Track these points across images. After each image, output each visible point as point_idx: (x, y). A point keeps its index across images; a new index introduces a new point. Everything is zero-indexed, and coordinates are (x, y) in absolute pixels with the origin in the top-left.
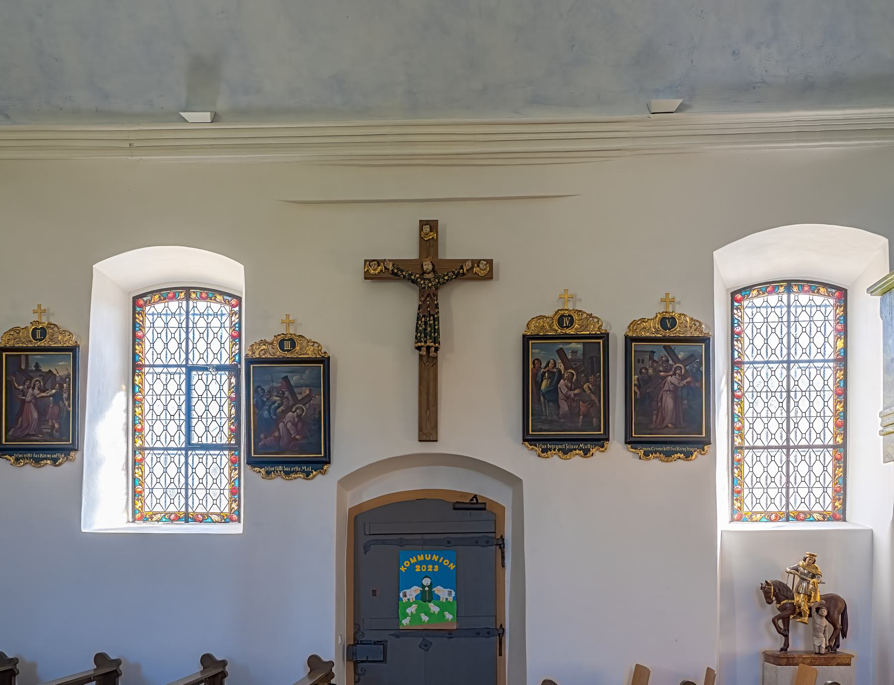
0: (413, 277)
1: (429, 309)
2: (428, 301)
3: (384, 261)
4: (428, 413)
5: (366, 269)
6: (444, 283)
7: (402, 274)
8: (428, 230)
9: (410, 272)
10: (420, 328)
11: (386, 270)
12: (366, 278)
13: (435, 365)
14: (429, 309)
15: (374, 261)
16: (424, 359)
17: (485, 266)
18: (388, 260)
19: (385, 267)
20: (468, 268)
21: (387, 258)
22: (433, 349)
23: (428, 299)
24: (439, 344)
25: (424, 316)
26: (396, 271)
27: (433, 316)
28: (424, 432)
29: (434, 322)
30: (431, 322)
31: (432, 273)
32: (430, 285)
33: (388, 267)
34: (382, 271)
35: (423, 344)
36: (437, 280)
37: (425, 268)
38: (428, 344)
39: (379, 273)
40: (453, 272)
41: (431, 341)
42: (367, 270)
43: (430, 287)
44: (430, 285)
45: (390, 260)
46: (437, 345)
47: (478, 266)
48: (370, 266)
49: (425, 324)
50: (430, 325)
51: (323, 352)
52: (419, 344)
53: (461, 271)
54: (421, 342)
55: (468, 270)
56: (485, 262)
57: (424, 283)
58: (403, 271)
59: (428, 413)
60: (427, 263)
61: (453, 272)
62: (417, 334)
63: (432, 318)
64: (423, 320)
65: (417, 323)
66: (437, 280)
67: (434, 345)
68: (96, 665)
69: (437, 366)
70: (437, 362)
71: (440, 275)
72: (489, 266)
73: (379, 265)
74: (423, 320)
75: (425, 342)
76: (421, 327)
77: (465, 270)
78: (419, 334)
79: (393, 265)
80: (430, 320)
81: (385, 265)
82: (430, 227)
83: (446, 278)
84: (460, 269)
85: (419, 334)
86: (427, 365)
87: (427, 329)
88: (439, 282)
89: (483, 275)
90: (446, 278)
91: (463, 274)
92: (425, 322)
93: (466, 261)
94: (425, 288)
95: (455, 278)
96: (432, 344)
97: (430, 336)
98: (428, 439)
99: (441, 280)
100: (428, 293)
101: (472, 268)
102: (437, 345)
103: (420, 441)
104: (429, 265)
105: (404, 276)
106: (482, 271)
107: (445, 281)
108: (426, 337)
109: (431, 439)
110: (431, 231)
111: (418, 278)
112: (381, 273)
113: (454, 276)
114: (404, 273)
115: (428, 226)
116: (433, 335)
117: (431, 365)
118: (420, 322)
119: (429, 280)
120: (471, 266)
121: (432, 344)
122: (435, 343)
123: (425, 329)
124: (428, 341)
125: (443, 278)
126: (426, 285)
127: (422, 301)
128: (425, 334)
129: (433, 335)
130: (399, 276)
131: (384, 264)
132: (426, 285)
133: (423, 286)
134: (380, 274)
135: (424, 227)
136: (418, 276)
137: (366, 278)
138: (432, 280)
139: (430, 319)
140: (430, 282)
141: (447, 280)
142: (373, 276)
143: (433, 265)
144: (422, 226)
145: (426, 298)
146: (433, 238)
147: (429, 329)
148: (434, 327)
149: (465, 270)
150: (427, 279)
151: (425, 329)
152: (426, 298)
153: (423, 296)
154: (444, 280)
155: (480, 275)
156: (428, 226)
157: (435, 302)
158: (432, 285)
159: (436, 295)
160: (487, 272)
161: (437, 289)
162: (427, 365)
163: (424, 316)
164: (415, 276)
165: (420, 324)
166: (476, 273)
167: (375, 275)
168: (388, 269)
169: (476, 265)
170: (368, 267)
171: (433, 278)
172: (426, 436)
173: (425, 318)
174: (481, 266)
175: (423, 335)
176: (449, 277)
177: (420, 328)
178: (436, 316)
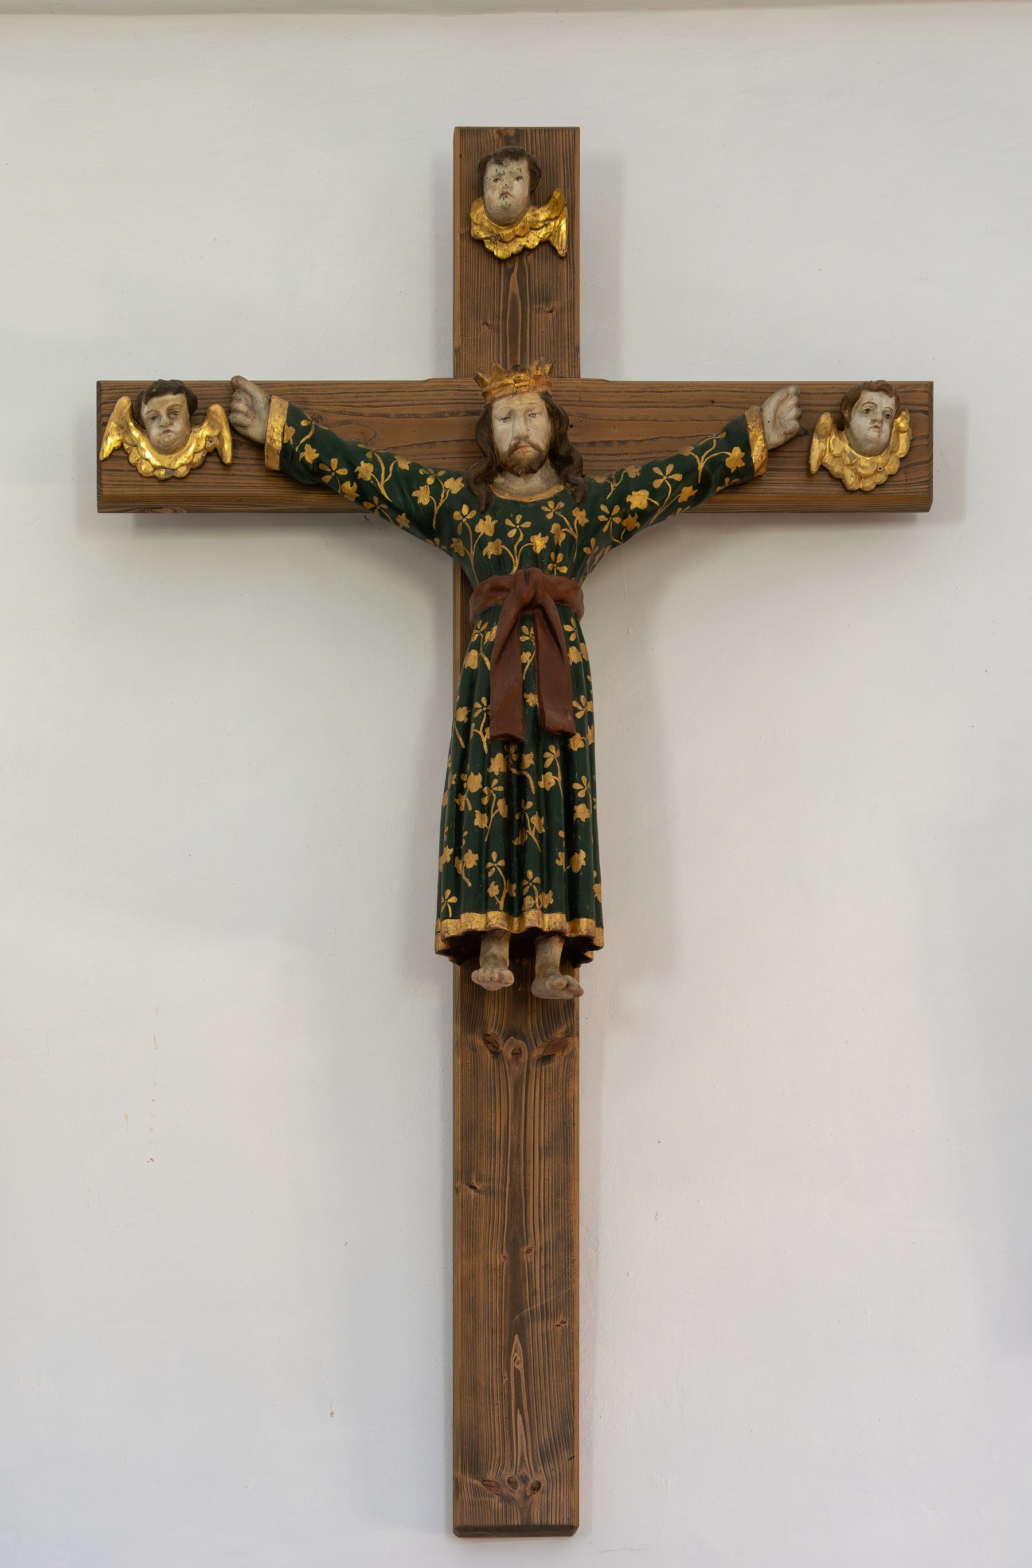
0: (423, 496)
1: (532, 699)
2: (525, 647)
3: (232, 389)
4: (517, 1355)
5: (111, 442)
6: (623, 535)
7: (353, 477)
8: (519, 190)
9: (404, 465)
10: (480, 821)
11: (243, 452)
12: (107, 503)
13: (559, 1056)
14: (532, 699)
15: (161, 388)
16: (493, 1016)
17: (886, 427)
18: (261, 385)
19: (233, 428)
20: (776, 438)
21: (254, 372)
22: (555, 951)
23: (527, 634)
24: (599, 924)
25: (504, 742)
26: (310, 455)
27: (564, 738)
28: (491, 1476)
29: (568, 779)
30: (551, 780)
31: (547, 471)
32: (539, 543)
33: (255, 432)
34: (213, 453)
35: (496, 918)
36: (580, 516)
37: (504, 434)
38: (532, 918)
39: (194, 469)
40: (685, 466)
41: (548, 899)
42: (120, 450)
43: (537, 560)
44: (539, 543)
45: (270, 388)
46: (585, 925)
47: (842, 425)
48: (141, 425)
49: (507, 796)
50: (544, 798)
51: (607, 519)
52: (475, 921)
53: (734, 457)
54: (484, 905)
55: (773, 452)
56: (886, 403)
57: (500, 532)
58: (361, 455)
59: (517, 1355)
60: (518, 404)
61: (685, 466)
62: (458, 853)
63: (552, 755)
64: (497, 765)
65: (457, 789)
66: (580, 516)
67: (567, 927)
68: (682, 502)
69: (573, 1056)
70: (573, 1032)
71: (600, 480)
72: (911, 424)
73: (196, 414)
74: (497, 765)
75: (514, 907)
76: (485, 810)
77: (757, 453)
78: (471, 859)
79: (293, 417)
80: (539, 770)
81: (239, 418)
82: (535, 173)
83: (639, 499)
84: (727, 445)
85: (471, 859)
86: (508, 1055)
87: (523, 825)
88: (592, 530)
89: (868, 484)
90: (639, 499)
91: (747, 475)
92: (506, 778)
93: (760, 392)
94: (501, 562)
95: (694, 501)
96: (555, 921)
97: (547, 870)
98: (517, 1521)
99: (608, 516)
100: (527, 595)
101: (803, 435)
102: (585, 925)
103: (464, 1530)
104: (530, 414)
105: (366, 492)
106: (864, 461)
107: (631, 522)
108: (514, 872)
109: (536, 1521)
110: (537, 197)
111: (455, 501)
112: (212, 466)
113: (688, 492)
114: (365, 470)
115: (521, 167)
116: (561, 861)
117: (537, 1053)
118: (474, 782)
119: (533, 511)
120: (792, 425)
121: (555, 921)
122: (573, 915)
123: (513, 825)
124: (528, 901)
125: (620, 498)
126: (510, 543)
127: (488, 650)
128: (507, 854)
129: (561, 861)
130: (331, 489)
131: (229, 411)
132: (510, 543)
133: (491, 550)
134: (195, 479)
135: (492, 170)
136: (453, 485)
137: (107, 503)
138: (550, 510)
139: (540, 760)
140: (542, 527)
141: (643, 516)
142: (158, 490)
143: (555, 414)
144: (482, 168)
145: (514, 631)
146: (545, 243)
147: (535, 824)
148: (570, 811)
149: (757, 453)
150: (515, 507)
151: (513, 825)
152: (514, 631)
153: (490, 615)
154: (626, 511)
155: (851, 481)
156: (521, 167)
157: (573, 656)
158: (552, 546)
159: (571, 610)
160: (893, 467)
161: (579, 568)
162: (508, 1055)
163: (504, 742)
164: (436, 490)
165: (481, 794)
166: (823, 468)
167: (172, 478)
168: (259, 447)
169: (826, 420)
170: (123, 429)
171: (556, 499)
172: (507, 1500)
173: (506, 754)
174: (860, 423)
175: (496, 863)
176: (653, 493)
177: (480, 821)
178: (576, 743)
